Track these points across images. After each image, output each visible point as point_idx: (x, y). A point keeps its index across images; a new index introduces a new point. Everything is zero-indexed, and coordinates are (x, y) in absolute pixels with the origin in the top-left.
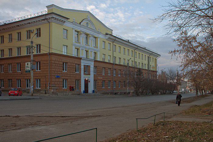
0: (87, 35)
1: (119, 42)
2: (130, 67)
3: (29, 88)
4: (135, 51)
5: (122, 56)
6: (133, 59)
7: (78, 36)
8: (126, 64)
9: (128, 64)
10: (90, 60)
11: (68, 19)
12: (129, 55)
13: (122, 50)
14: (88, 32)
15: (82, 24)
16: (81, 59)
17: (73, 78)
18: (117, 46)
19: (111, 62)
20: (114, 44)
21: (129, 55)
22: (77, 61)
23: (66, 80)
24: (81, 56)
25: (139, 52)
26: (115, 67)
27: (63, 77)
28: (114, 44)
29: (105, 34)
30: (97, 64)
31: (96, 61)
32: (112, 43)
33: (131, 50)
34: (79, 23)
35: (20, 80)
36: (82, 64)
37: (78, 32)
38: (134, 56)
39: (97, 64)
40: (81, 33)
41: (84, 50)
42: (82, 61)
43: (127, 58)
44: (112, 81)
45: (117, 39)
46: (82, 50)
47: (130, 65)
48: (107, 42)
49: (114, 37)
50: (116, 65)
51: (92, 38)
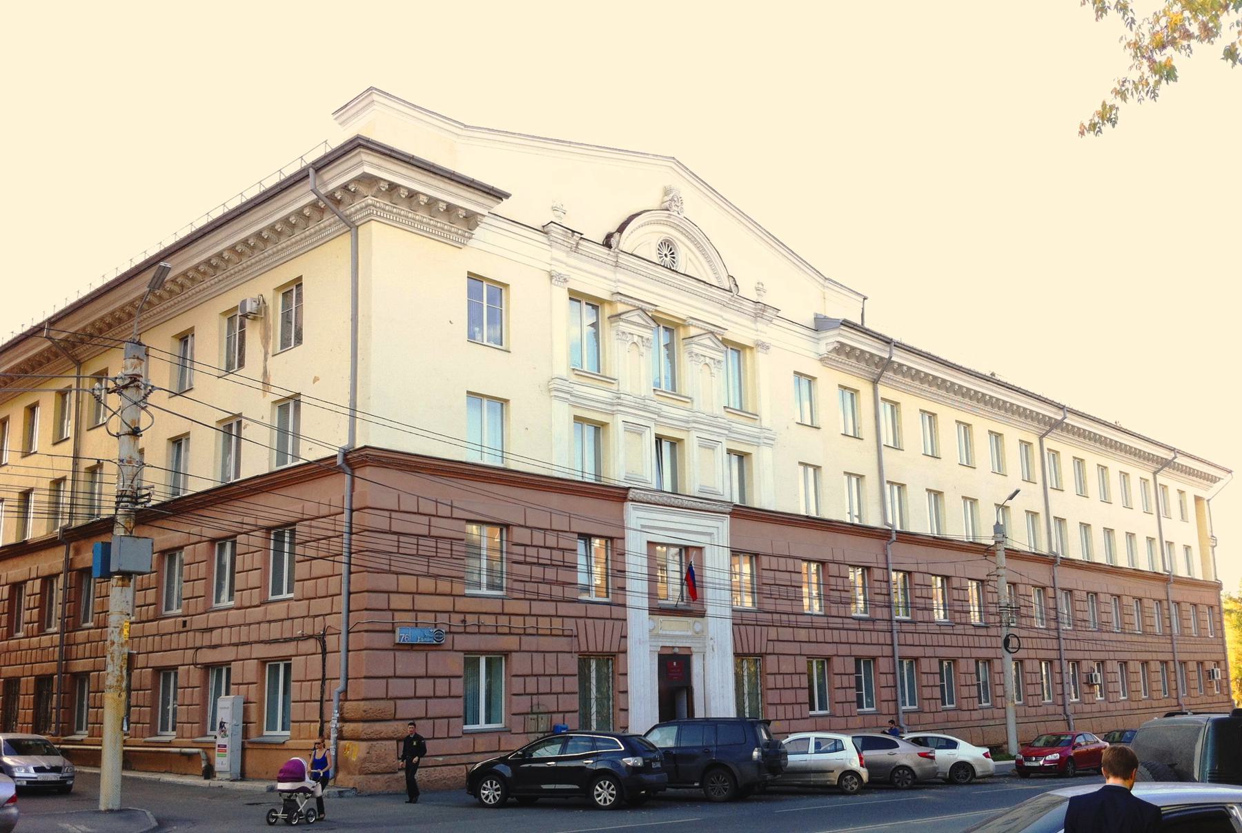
0: (671, 326)
1: (916, 375)
2: (1013, 554)
3: (279, 732)
4: (1049, 443)
5: (1099, 515)
6: (1031, 498)
7: (597, 335)
8: (986, 537)
9: (999, 528)
10: (704, 505)
11: (499, 195)
12: (1000, 470)
13: (982, 444)
14: (674, 304)
15: (627, 241)
16: (619, 495)
17: (562, 644)
18: (912, 405)
19: (1120, 564)
20: (884, 391)
21: (1000, 470)
22: (589, 512)
23: (496, 658)
24: (616, 474)
25: (1104, 461)
26: (1066, 578)
27: (463, 642)
28: (884, 391)
29: (809, 320)
30: (762, 537)
31: (742, 513)
32: (865, 389)
33: (1013, 434)
34: (601, 239)
35: (288, 668)
36: (635, 544)
37: (596, 304)
38: (1039, 479)
39: (762, 537)
40: (621, 308)
41: (721, 451)
42: (634, 516)
43: (990, 490)
44: (884, 664)
45: (899, 357)
46: (708, 445)
47: (1020, 540)
48: (829, 380)
49: (1054, 410)
50: (1070, 563)
51: (636, 328)
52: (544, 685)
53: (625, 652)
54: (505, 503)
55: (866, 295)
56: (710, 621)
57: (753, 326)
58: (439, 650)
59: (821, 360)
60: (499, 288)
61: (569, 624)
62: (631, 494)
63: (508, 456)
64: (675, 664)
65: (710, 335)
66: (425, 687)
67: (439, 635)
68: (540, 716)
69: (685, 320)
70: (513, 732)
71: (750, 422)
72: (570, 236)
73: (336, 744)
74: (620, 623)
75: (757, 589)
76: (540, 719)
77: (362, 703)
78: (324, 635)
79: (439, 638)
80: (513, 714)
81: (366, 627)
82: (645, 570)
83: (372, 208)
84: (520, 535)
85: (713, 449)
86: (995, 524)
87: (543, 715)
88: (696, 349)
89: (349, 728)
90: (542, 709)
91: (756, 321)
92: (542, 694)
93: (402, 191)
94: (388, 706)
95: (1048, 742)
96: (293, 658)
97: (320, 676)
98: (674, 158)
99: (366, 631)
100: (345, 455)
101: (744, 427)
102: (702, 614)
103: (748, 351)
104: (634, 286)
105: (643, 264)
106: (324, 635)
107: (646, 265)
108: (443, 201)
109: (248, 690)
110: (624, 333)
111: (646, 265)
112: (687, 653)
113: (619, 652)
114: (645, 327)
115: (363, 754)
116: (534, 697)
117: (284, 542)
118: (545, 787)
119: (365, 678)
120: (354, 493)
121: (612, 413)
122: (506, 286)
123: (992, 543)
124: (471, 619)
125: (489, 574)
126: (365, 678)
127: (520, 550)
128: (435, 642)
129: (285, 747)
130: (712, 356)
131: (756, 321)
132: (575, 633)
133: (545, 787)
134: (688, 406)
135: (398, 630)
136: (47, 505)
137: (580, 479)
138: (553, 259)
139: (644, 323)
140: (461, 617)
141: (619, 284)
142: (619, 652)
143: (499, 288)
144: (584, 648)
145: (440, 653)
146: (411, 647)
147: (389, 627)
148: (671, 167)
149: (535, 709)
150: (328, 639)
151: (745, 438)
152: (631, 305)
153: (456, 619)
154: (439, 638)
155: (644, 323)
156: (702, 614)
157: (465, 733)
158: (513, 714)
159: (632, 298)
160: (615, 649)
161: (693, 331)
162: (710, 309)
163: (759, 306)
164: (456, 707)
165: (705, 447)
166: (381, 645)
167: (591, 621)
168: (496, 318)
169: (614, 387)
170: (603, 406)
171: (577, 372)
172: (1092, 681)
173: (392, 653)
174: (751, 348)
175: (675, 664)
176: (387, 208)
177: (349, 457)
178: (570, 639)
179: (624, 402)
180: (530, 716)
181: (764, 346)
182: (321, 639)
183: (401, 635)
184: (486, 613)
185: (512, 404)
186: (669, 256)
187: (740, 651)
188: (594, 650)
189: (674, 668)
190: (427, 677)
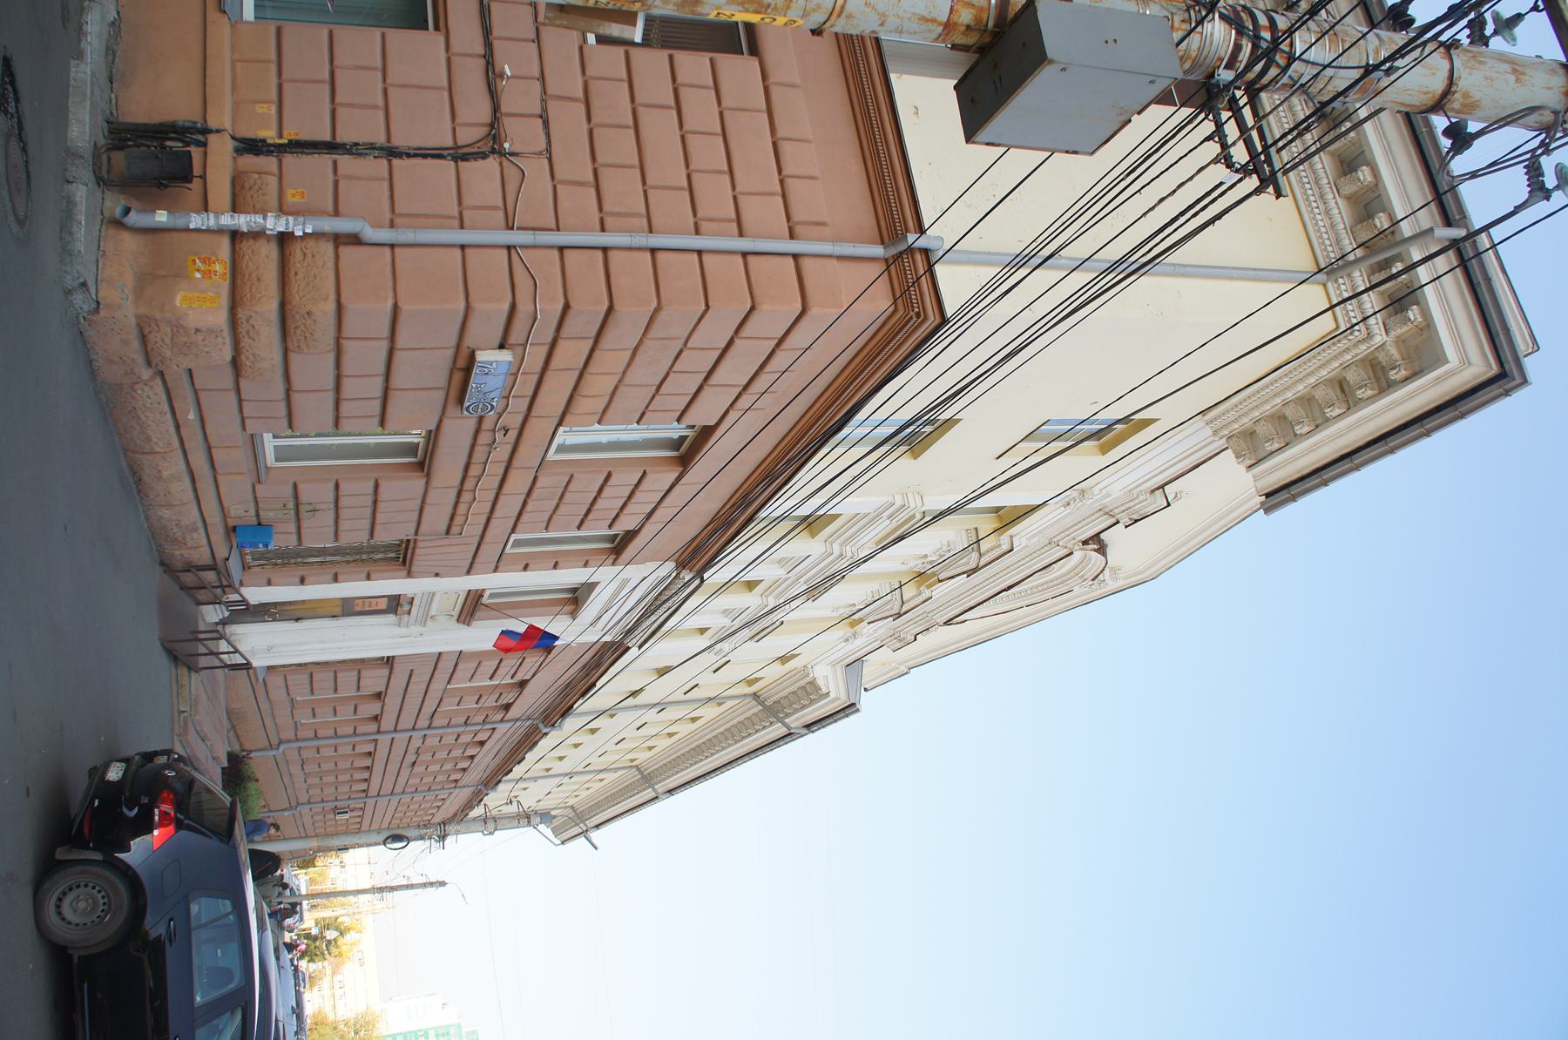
70: (258, 487)
71: (833, 658)
73: (220, 231)
77: (331, 306)
78: (502, 153)
80: (295, 486)
81: (524, 308)
89: (265, 258)
95: (254, 239)
96: (441, 38)
97: (399, 141)
99: (513, 307)
100: (926, 252)
106: (502, 153)
109: (371, 69)
115: (193, 320)
118: (86, 985)
119: (396, 307)
120: (835, 261)
126: (396, 307)
129: (213, 14)
133: (86, 985)
135: (505, 356)
136: (1313, 297)
150: (492, 163)
158: (295, 486)
172: (339, 813)
177: (918, 257)
182: (493, 144)
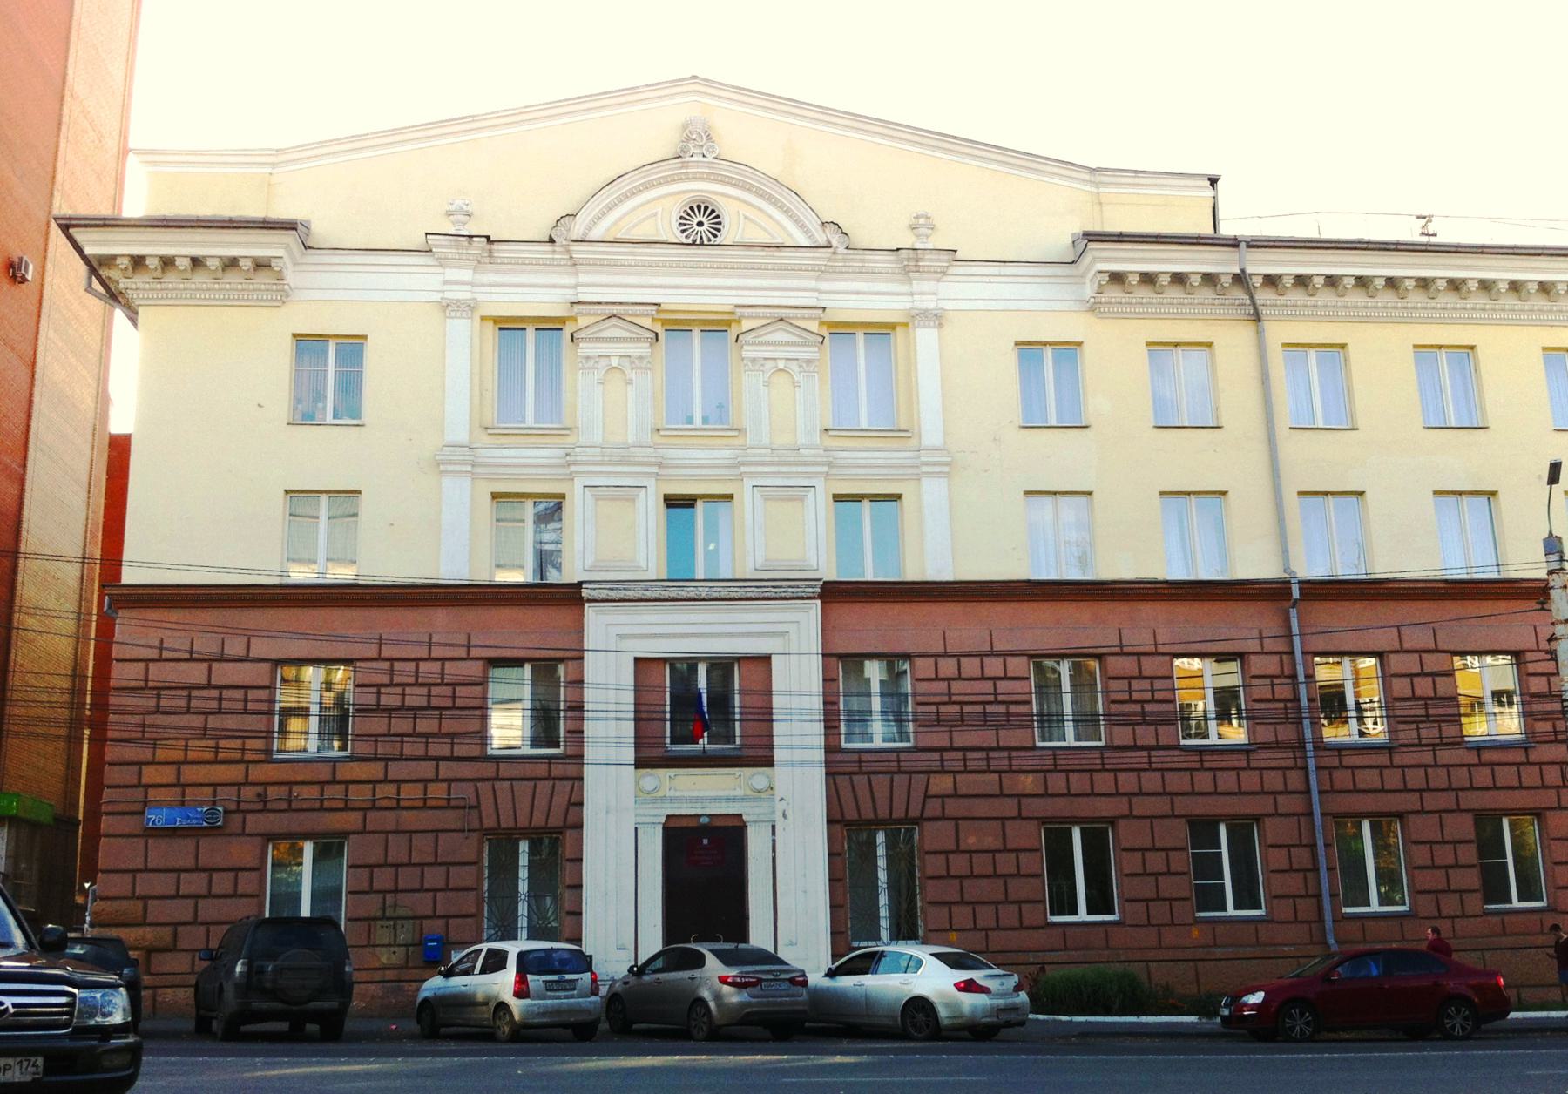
16: (571, 597)
20: (1279, 332)
42: (598, 624)
52: (408, 878)
53: (579, 826)
54: (1379, 623)
55: (1213, 172)
56: (779, 774)
57: (905, 288)
58: (220, 835)
59: (1092, 310)
60: (352, 347)
61: (463, 792)
62: (585, 593)
63: (1505, 568)
64: (705, 841)
65: (781, 325)
66: (434, 877)
67: (212, 813)
68: (399, 922)
69: (733, 313)
72: (466, 244)
74: (568, 784)
75: (741, 713)
76: (399, 927)
79: (212, 819)
82: (632, 708)
83: (1098, 306)
84: (1397, 663)
85: (802, 499)
86: (1546, 535)
87: (404, 922)
88: (749, 351)
90: (401, 912)
91: (910, 281)
92: (402, 891)
93: (1530, 286)
94: (136, 907)
98: (695, 77)
101: (877, 454)
102: (768, 762)
103: (899, 330)
104: (858, 293)
105: (808, 255)
107: (812, 255)
108: (1561, 282)
110: (588, 358)
111: (812, 255)
112: (736, 823)
113: (566, 827)
114: (804, 345)
116: (388, 896)
117: (740, 707)
121: (571, 478)
122: (365, 337)
123: (1542, 574)
124: (273, 792)
125: (884, 717)
127: (1123, 685)
128: (205, 824)
130: (790, 355)
131: (910, 281)
132: (473, 802)
134: (736, 442)
137: (1495, 576)
138: (446, 282)
139: (795, 339)
140: (260, 789)
141: (579, 289)
142: (566, 827)
143: (352, 347)
144: (489, 822)
145: (220, 840)
146: (172, 832)
147: (139, 807)
148: (695, 91)
149: (389, 913)
151: (533, 471)
152: (764, 317)
153: (249, 793)
154: (212, 819)
155: (795, 339)
156: (768, 762)
157: (1487, 913)
159: (599, 303)
160: (556, 821)
161: (746, 325)
162: (795, 283)
163: (903, 254)
164: (1183, 886)
165: (782, 500)
166: (126, 831)
167: (506, 784)
168: (351, 385)
169: (913, 442)
170: (553, 471)
171: (662, 433)
173: (141, 841)
174: (906, 325)
175: (705, 841)
176: (1488, 306)
178: (462, 811)
179: (578, 458)
180: (380, 923)
181: (937, 318)
183: (155, 817)
184: (303, 783)
185: (1501, 496)
186: (697, 228)
187: (851, 814)
188: (511, 824)
189: (705, 847)
190: (196, 869)
